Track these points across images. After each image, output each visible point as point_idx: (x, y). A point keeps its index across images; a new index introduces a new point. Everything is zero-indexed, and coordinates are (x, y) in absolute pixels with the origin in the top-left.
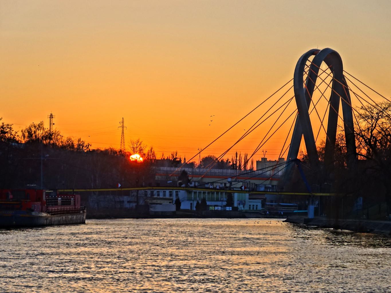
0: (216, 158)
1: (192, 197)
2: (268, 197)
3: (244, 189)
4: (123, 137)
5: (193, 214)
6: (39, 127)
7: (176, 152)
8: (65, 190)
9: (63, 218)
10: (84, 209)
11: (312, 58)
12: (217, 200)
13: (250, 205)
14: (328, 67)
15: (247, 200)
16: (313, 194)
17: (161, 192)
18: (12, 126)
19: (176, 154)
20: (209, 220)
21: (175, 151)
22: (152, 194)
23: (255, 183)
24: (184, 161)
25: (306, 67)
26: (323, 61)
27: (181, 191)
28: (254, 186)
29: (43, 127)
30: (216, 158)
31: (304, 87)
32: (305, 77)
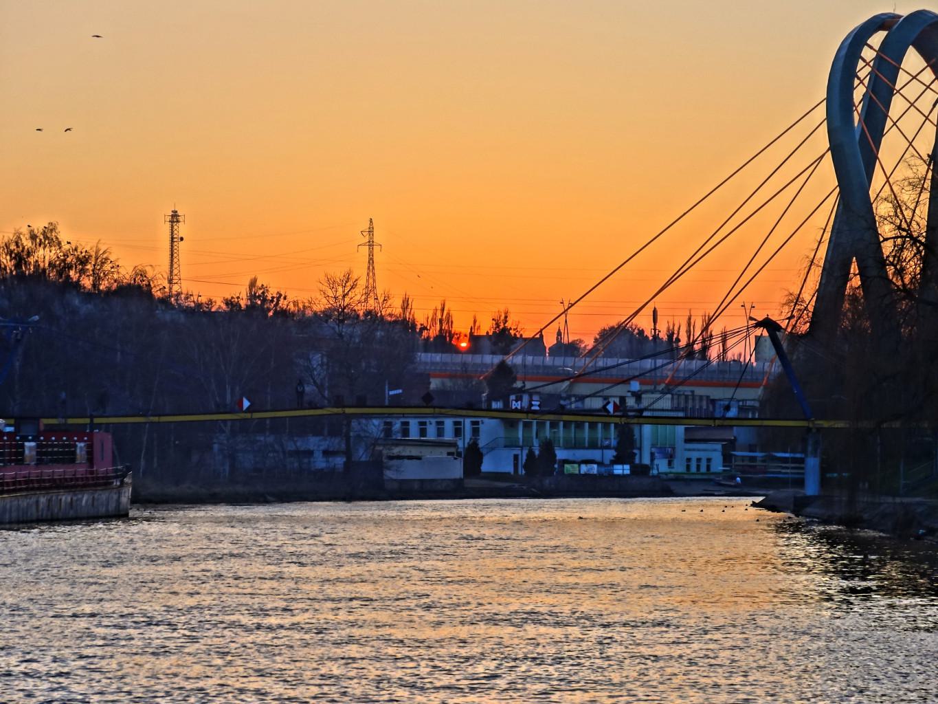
0: (638, 329)
1: (519, 438)
2: (741, 434)
3: (614, 412)
4: (371, 274)
5: (517, 485)
6: (46, 238)
7: (506, 313)
8: (70, 421)
9: (37, 502)
10: (124, 476)
11: (877, 39)
12: (593, 445)
13: (689, 460)
14: (926, 65)
15: (680, 444)
16: (816, 422)
19: (506, 317)
20: (509, 505)
21: (502, 309)
22: (388, 431)
23: (708, 397)
24: (557, 339)
25: (861, 64)
26: (911, 46)
27: (486, 420)
28: (708, 406)
29: (57, 238)
30: (638, 329)
31: (856, 124)
32: (859, 93)
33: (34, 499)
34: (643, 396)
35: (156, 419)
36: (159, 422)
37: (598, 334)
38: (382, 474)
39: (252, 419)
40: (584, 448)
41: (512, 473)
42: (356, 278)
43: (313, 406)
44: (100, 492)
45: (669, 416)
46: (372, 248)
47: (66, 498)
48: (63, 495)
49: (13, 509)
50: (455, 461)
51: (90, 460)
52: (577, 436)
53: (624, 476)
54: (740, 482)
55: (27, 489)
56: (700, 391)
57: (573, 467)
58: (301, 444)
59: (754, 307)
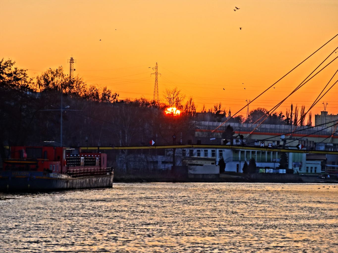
2: (329, 157)
3: (302, 148)
4: (156, 86)
5: (240, 177)
9: (86, 180)
10: (111, 171)
12: (269, 161)
13: (308, 168)
15: (304, 161)
19: (220, 106)
21: (219, 103)
23: (313, 141)
24: (229, 115)
27: (225, 150)
29: (62, 73)
30: (267, 111)
33: (85, 180)
34: (287, 141)
35: (117, 148)
36: (118, 149)
37: (120, 100)
38: (187, 171)
39: (155, 149)
40: (265, 162)
41: (236, 171)
42: (179, 91)
44: (105, 177)
45: (204, 146)
46: (157, 75)
47: (94, 179)
48: (94, 178)
49: (79, 183)
50: (216, 167)
51: (100, 165)
52: (262, 157)
53: (283, 174)
54: (329, 177)
55: (83, 176)
56: (310, 139)
57: (263, 170)
58: (155, 159)
59: (328, 104)
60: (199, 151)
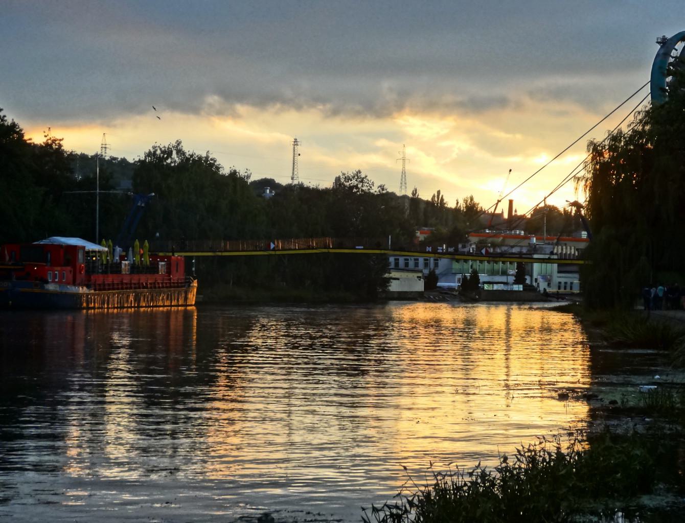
4: (404, 176)
17: (411, 260)
18: (61, 142)
21: (383, 184)
28: (574, 251)
36: (275, 254)
43: (313, 248)
51: (169, 272)
60: (408, 260)
